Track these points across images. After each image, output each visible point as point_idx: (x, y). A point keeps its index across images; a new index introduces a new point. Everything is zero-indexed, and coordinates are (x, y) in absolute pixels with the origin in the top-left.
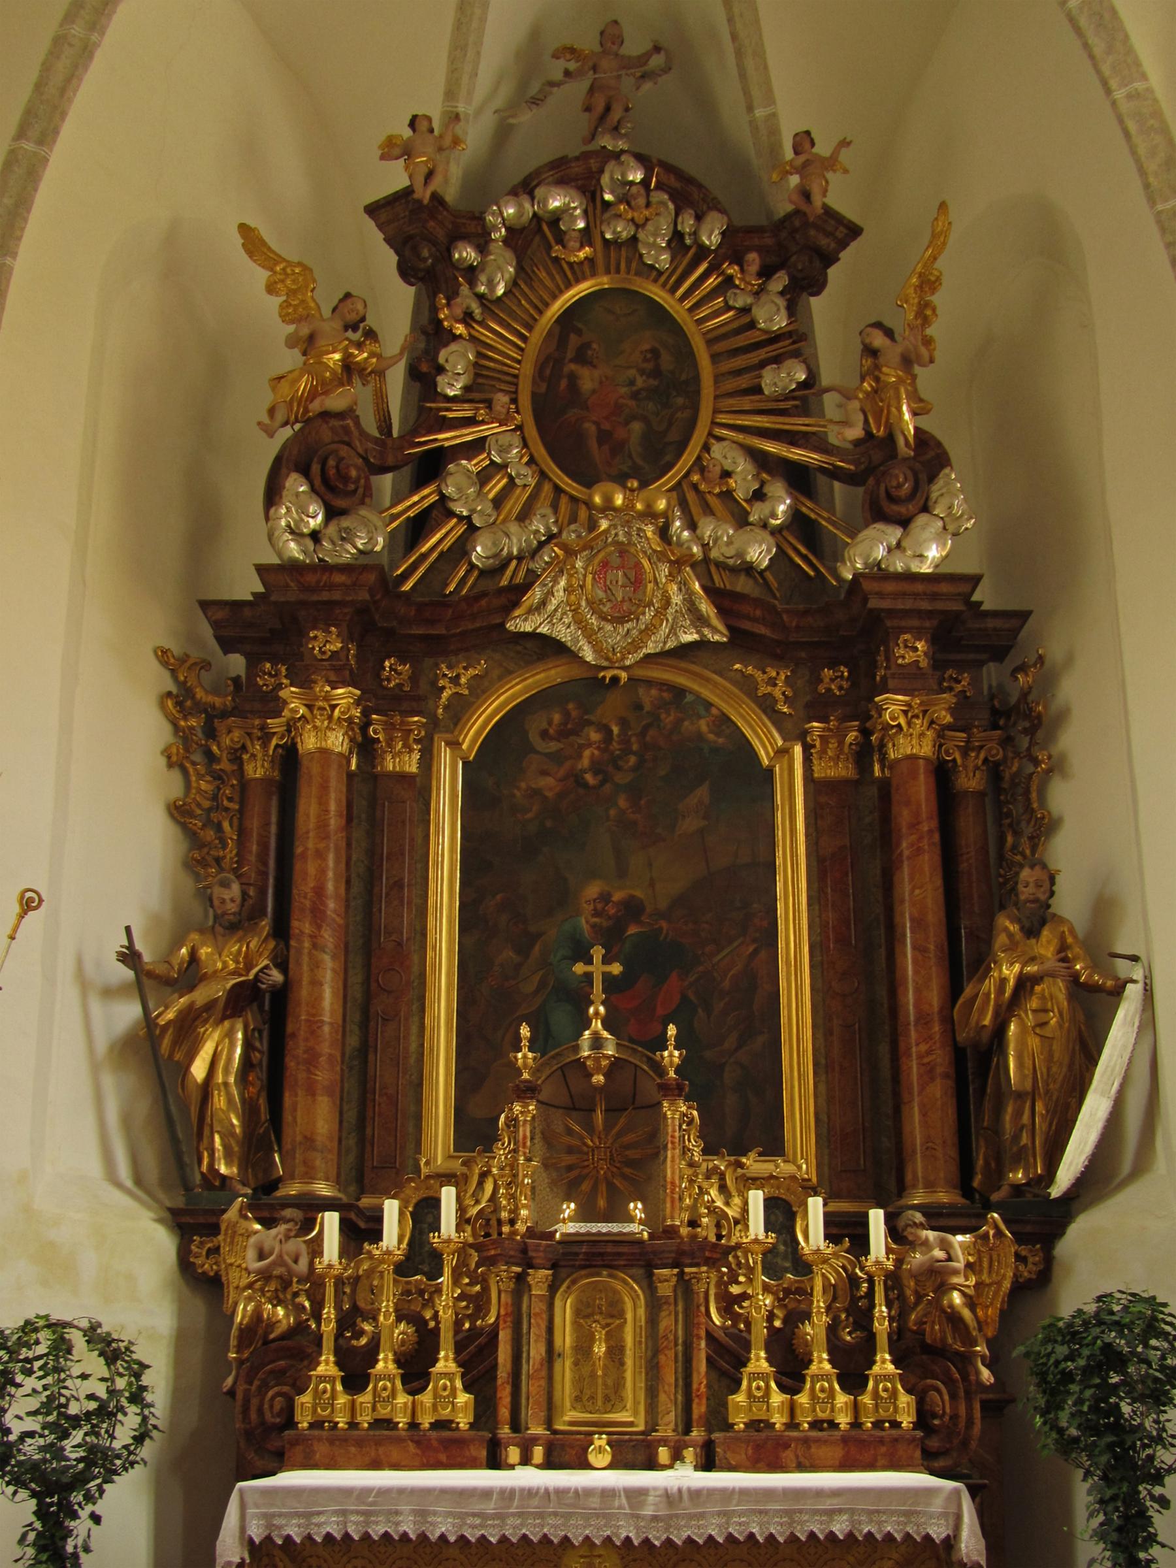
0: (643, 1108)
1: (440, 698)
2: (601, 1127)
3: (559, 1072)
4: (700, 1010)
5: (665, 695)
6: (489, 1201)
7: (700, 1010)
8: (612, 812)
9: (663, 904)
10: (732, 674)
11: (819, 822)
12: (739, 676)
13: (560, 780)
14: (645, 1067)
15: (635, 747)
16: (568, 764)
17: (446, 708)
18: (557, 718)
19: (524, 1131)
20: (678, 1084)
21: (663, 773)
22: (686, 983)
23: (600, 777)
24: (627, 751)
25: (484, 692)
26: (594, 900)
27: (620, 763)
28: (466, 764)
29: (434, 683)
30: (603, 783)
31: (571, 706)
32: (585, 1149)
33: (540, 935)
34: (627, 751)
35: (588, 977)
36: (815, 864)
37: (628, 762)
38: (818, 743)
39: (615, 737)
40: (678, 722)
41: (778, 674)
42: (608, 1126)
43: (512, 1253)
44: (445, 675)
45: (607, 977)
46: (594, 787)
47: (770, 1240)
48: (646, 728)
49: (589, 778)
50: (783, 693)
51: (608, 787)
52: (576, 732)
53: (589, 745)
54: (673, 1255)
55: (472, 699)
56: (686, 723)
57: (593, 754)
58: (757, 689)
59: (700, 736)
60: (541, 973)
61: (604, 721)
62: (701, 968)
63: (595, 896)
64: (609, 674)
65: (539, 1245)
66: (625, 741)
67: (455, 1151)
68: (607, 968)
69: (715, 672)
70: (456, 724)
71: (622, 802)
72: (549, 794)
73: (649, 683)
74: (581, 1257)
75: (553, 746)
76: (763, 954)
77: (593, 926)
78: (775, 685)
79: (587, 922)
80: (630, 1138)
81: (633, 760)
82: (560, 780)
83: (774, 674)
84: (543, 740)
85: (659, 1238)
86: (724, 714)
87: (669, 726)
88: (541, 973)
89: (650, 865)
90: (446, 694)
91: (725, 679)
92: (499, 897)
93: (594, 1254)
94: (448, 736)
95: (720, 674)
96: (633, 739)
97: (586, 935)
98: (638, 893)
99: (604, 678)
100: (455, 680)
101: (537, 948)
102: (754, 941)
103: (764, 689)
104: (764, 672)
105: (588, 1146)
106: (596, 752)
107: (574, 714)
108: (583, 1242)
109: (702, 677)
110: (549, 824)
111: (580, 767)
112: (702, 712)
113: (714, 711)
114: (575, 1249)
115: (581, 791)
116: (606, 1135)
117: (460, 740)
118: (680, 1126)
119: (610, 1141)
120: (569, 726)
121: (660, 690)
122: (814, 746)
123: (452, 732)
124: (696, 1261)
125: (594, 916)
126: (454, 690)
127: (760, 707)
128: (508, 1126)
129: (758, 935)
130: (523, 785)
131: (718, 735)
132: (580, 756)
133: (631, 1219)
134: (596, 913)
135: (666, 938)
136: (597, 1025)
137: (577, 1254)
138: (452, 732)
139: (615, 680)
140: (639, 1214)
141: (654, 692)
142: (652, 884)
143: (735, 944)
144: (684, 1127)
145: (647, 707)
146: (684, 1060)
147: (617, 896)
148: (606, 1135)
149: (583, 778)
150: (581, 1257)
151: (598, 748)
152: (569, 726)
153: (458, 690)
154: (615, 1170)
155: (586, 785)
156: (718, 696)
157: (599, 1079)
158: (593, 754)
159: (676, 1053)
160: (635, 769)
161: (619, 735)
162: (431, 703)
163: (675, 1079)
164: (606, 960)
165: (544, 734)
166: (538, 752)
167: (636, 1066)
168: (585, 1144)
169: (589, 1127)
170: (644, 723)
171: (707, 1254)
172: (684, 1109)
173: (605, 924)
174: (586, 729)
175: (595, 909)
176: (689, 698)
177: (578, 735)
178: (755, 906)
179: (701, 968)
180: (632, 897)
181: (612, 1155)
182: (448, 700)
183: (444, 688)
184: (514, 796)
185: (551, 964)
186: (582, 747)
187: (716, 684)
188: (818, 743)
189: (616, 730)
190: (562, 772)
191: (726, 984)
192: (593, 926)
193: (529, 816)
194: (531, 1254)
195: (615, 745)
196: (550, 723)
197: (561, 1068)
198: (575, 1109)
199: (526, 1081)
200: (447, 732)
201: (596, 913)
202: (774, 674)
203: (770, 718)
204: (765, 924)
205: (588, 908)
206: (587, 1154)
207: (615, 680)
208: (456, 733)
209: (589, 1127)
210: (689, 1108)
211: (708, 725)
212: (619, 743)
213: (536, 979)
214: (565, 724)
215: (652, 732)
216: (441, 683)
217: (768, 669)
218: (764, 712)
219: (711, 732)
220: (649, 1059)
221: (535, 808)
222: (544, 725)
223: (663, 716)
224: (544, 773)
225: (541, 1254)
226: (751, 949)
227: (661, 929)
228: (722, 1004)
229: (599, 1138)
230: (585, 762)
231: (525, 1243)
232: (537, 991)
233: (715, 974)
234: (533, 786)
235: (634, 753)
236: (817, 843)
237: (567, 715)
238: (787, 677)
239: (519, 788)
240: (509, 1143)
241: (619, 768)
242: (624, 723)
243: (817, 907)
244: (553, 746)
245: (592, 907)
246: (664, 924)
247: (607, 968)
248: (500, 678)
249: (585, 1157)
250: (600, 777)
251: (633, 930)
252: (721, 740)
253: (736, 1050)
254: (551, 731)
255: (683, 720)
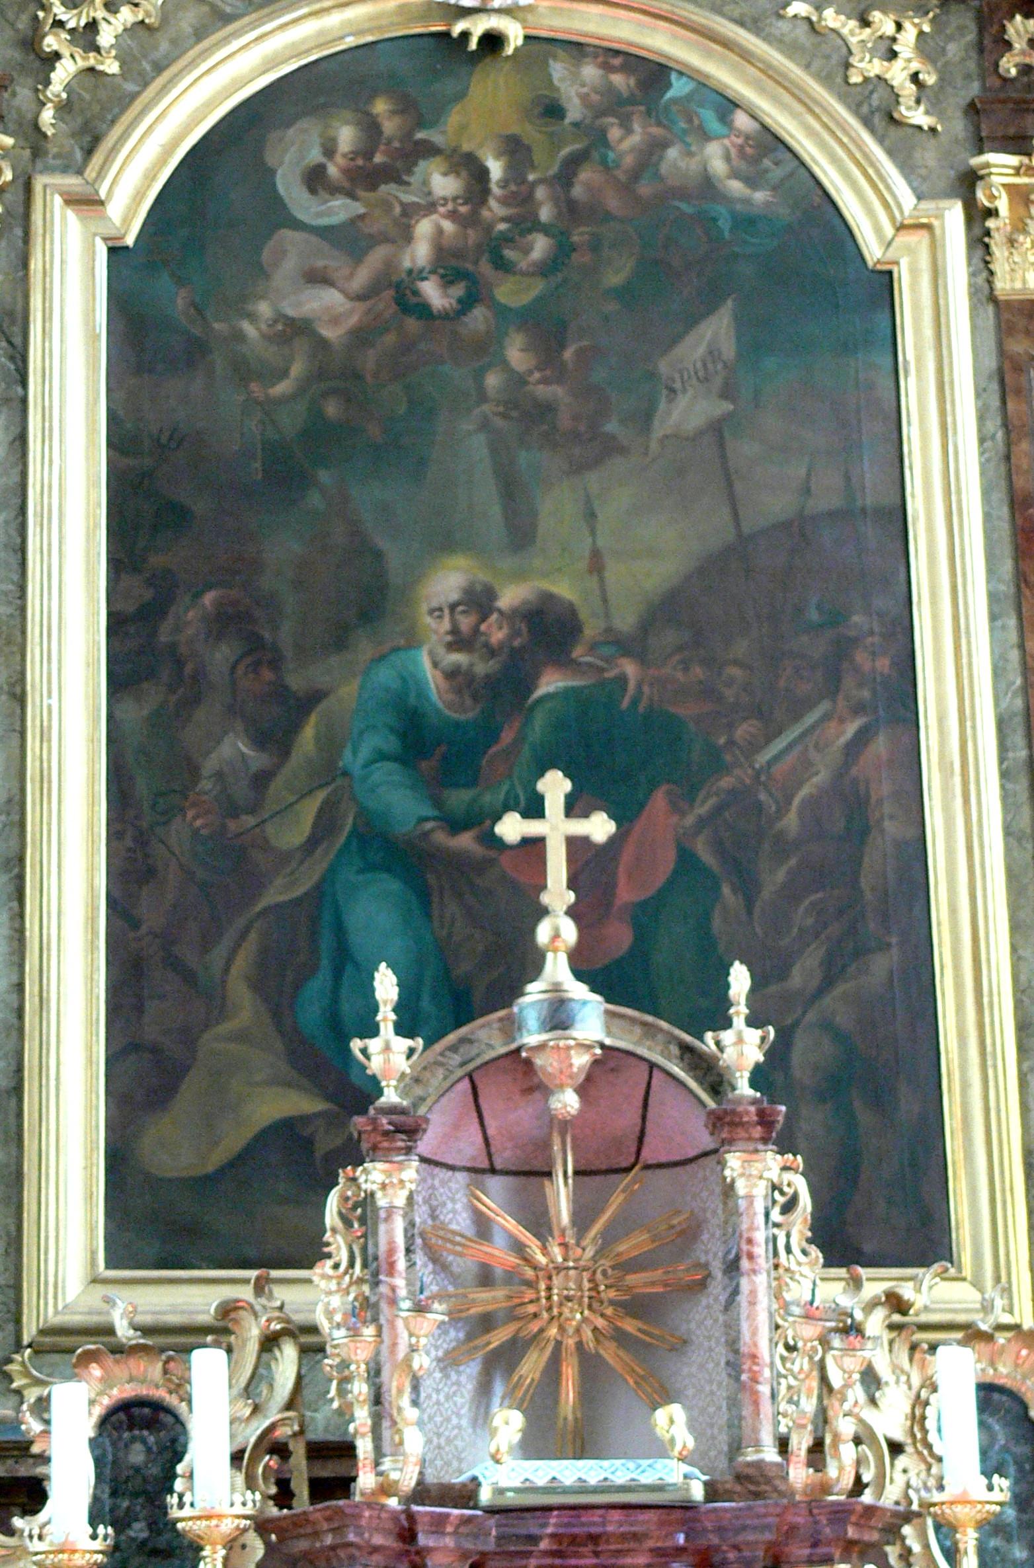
0: (660, 1166)
1: (47, 83)
2: (565, 1218)
3: (465, 1084)
4: (726, 890)
5: (618, 79)
6: (289, 1406)
7: (726, 890)
8: (493, 381)
9: (626, 620)
10: (784, 26)
11: (1011, 406)
12: (802, 30)
13: (360, 297)
14: (677, 1070)
15: (545, 214)
16: (377, 257)
17: (64, 109)
18: (346, 136)
19: (390, 1232)
20: (761, 1113)
21: (614, 278)
22: (690, 820)
23: (458, 290)
24: (525, 223)
25: (159, 68)
26: (453, 607)
27: (509, 253)
28: (115, 252)
29: (31, 43)
30: (466, 304)
31: (381, 107)
32: (529, 1273)
33: (315, 697)
34: (525, 223)
35: (534, 846)
36: (1005, 511)
37: (527, 251)
38: (1003, 204)
39: (495, 189)
40: (656, 147)
41: (899, 27)
42: (582, 1218)
43: (378, 1540)
44: (59, 24)
45: (575, 845)
46: (445, 316)
47: (997, 1496)
48: (574, 163)
49: (432, 292)
50: (915, 77)
51: (479, 317)
52: (393, 174)
53: (431, 207)
54: (769, 1536)
55: (130, 87)
56: (672, 153)
57: (440, 231)
58: (847, 66)
59: (708, 186)
60: (321, 795)
61: (466, 147)
62: (726, 782)
63: (455, 596)
64: (478, 27)
65: (442, 1520)
66: (521, 198)
67: (109, 1265)
68: (579, 827)
69: (741, 23)
70: (89, 152)
71: (517, 354)
72: (330, 333)
73: (577, 49)
74: (544, 1545)
75: (339, 210)
76: (880, 745)
77: (452, 674)
78: (893, 55)
79: (435, 665)
80: (626, 1247)
81: (540, 246)
82: (360, 297)
83: (889, 28)
84: (313, 191)
85: (729, 1496)
86: (765, 128)
87: (629, 161)
88: (321, 795)
89: (591, 516)
90: (63, 73)
91: (768, 39)
92: (209, 598)
93: (574, 1540)
94: (71, 182)
95: (754, 24)
96: (541, 193)
97: (434, 696)
98: (564, 590)
99: (465, 35)
100: (87, 36)
101: (309, 733)
102: (858, 709)
103: (867, 66)
104: (865, 23)
105: (535, 1267)
106: (448, 226)
107: (390, 127)
108: (548, 1509)
109: (726, 44)
110: (332, 409)
111: (407, 264)
112: (713, 124)
113: (741, 120)
114: (531, 1526)
115: (412, 324)
116: (580, 1236)
117: (103, 194)
118: (767, 1215)
119: (590, 1252)
120: (378, 159)
121: (607, 68)
122: (992, 213)
123: (80, 172)
124: (822, 1550)
125: (451, 647)
126: (81, 64)
127: (856, 109)
128: (347, 1223)
129: (866, 694)
130: (264, 309)
131: (752, 182)
132: (407, 236)
133: (660, 1450)
134: (459, 642)
135: (635, 702)
136: (557, 968)
137: (533, 1539)
138: (80, 172)
139: (493, 41)
140: (684, 1439)
141: (590, 72)
142: (596, 564)
143: (810, 719)
144: (776, 1215)
145: (574, 111)
146: (777, 1056)
147: (510, 597)
148: (580, 1236)
149: (416, 293)
150: (544, 1545)
151: (453, 215)
152: (378, 159)
153: (92, 60)
154: (600, 1323)
155: (423, 310)
156: (749, 82)
157: (568, 1102)
158: (440, 231)
159: (753, 1035)
160: (545, 269)
161: (504, 183)
162: (23, 94)
163: (754, 1102)
164: (574, 807)
165: (315, 179)
166: (298, 225)
167: (652, 1066)
168: (528, 1261)
169: (539, 1223)
170: (565, 151)
171: (851, 1532)
172: (774, 1174)
173: (482, 668)
174: (422, 165)
175: (455, 631)
176: (679, 88)
177: (400, 182)
178: (856, 618)
179: (726, 782)
180: (548, 598)
181: (595, 1288)
182: (68, 88)
183: (57, 56)
184: (240, 337)
185: (345, 773)
186: (410, 212)
187: (746, 55)
188: (1003, 204)
189: (496, 168)
190: (362, 277)
191: (791, 822)
192: (452, 674)
193: (281, 388)
194: (423, 1540)
195: (495, 208)
196: (329, 151)
197: (470, 1076)
198: (493, 1171)
199: (393, 1110)
200: (65, 170)
201: (459, 642)
202: (889, 28)
203: (881, 140)
204: (883, 664)
205: (437, 629)
206: (531, 1284)
207: (493, 41)
208: (91, 172)
209: (539, 1223)
210: (785, 1168)
211: (727, 158)
212: (504, 201)
213: (309, 810)
214: (368, 154)
215: (586, 175)
216: (51, 43)
217: (876, 16)
218: (867, 122)
219: (735, 174)
220: (686, 1049)
221: (297, 369)
222: (315, 155)
223: (615, 133)
224: (317, 278)
225: (449, 1542)
226: (851, 729)
227: (622, 680)
228: (781, 875)
229: (564, 1245)
230: (421, 252)
231: (411, 1517)
232: (312, 843)
233: (763, 796)
234: (291, 312)
235: (545, 229)
236: (1008, 458)
237: (371, 128)
238: (921, 33)
239: (252, 317)
240: (351, 1264)
241: (502, 265)
242: (514, 149)
243: (1012, 622)
244: (339, 210)
245: (446, 625)
246: (630, 668)
247: (579, 827)
248: (200, 34)
249: (530, 1294)
250: (458, 290)
251: (551, 683)
252: (760, 196)
253: (821, 992)
254: (333, 170)
255: (664, 145)
